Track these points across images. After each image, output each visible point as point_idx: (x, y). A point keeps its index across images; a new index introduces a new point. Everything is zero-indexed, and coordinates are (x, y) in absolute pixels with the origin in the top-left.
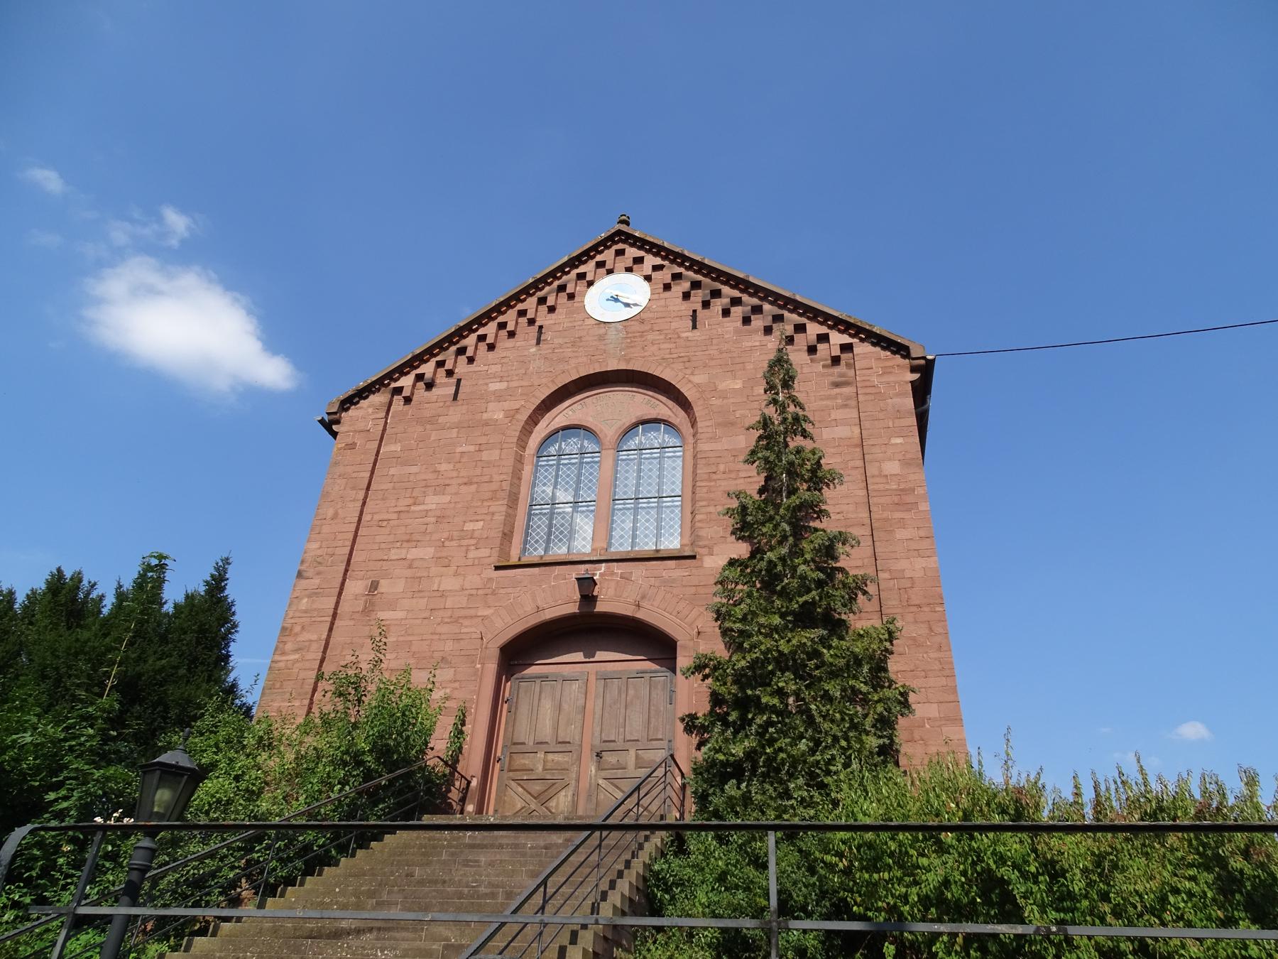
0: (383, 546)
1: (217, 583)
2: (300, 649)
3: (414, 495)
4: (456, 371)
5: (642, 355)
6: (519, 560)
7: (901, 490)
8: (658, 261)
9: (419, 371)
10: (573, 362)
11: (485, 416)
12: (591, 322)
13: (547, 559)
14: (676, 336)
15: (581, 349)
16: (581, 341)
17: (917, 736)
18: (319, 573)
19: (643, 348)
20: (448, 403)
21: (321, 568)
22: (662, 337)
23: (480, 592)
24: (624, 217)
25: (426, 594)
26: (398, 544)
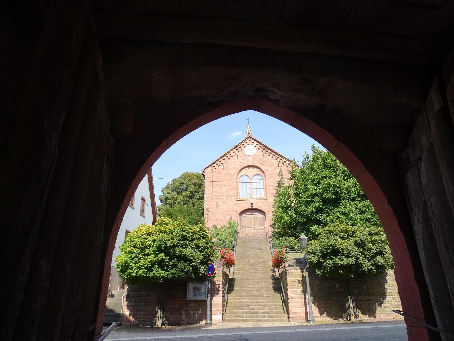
18: (208, 201)
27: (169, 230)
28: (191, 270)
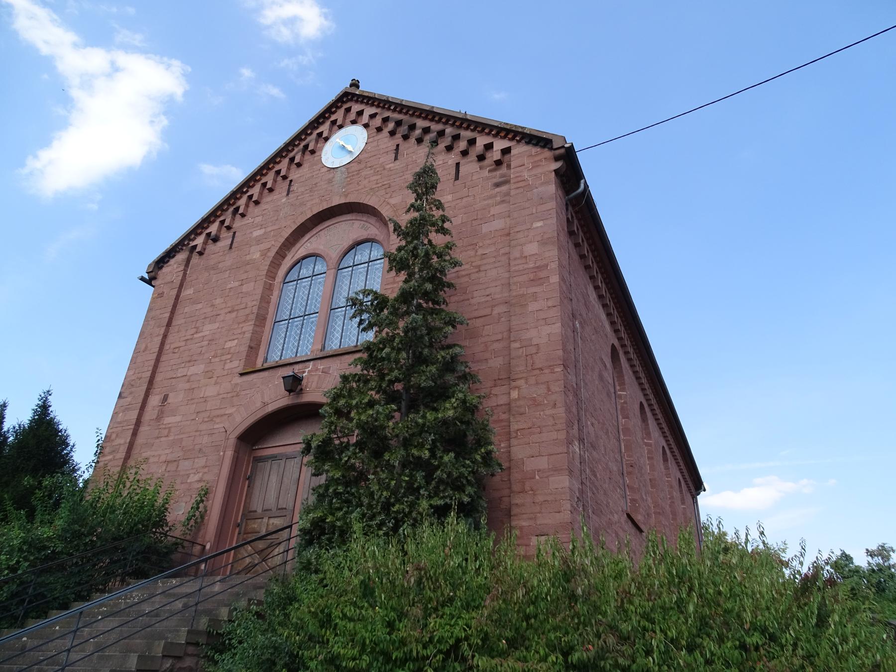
0: (174, 367)
1: (44, 408)
2: (114, 451)
3: (197, 325)
4: (234, 226)
5: (356, 189)
6: (262, 365)
7: (537, 267)
8: (373, 110)
9: (208, 231)
10: (309, 204)
11: (248, 257)
12: (325, 170)
13: (281, 363)
14: (382, 169)
15: (316, 192)
16: (316, 187)
17: (527, 488)
18: (131, 393)
19: (358, 184)
20: (226, 252)
21: (133, 389)
22: (372, 171)
23: (229, 395)
24: (354, 81)
25: (196, 401)
26: (183, 364)
27: (336, 580)
28: (314, 529)
